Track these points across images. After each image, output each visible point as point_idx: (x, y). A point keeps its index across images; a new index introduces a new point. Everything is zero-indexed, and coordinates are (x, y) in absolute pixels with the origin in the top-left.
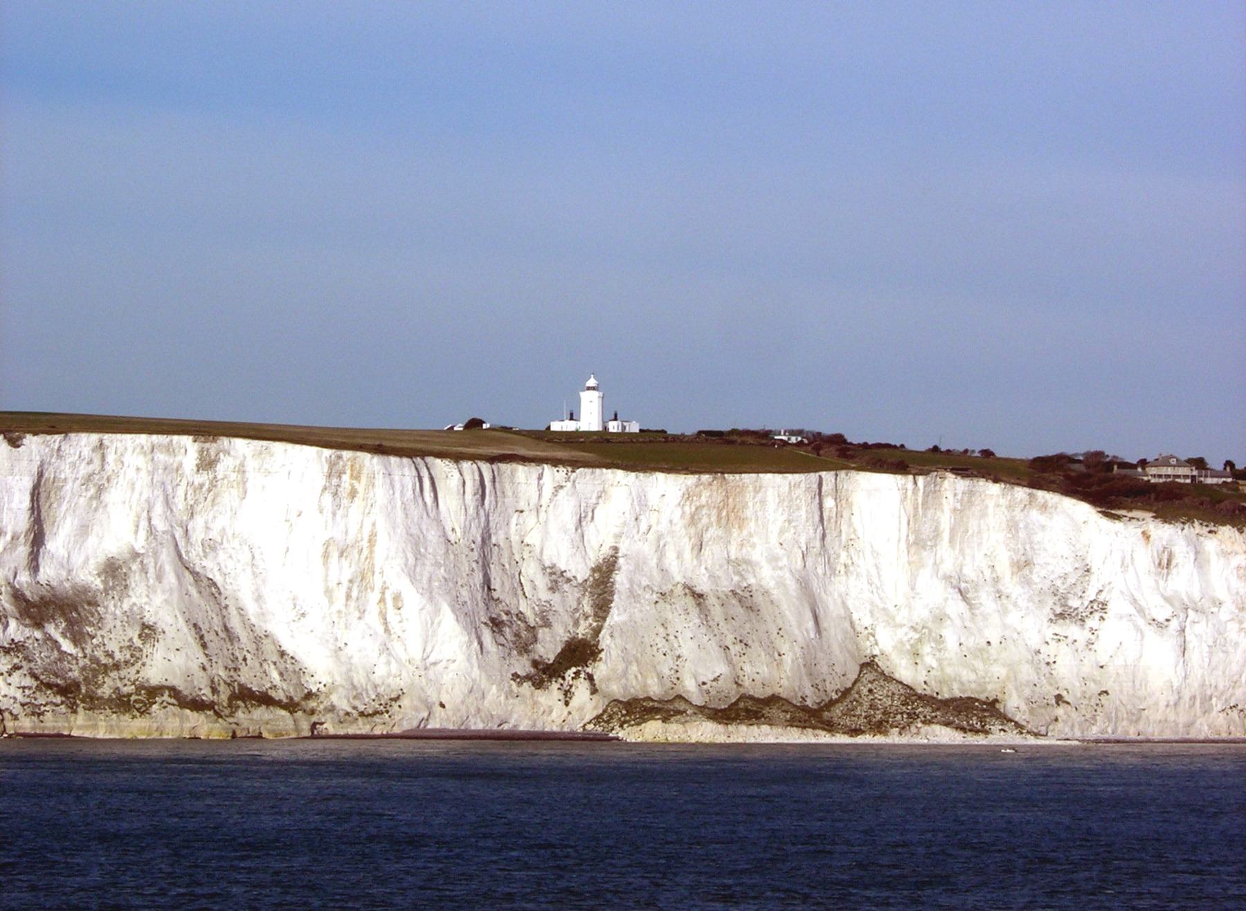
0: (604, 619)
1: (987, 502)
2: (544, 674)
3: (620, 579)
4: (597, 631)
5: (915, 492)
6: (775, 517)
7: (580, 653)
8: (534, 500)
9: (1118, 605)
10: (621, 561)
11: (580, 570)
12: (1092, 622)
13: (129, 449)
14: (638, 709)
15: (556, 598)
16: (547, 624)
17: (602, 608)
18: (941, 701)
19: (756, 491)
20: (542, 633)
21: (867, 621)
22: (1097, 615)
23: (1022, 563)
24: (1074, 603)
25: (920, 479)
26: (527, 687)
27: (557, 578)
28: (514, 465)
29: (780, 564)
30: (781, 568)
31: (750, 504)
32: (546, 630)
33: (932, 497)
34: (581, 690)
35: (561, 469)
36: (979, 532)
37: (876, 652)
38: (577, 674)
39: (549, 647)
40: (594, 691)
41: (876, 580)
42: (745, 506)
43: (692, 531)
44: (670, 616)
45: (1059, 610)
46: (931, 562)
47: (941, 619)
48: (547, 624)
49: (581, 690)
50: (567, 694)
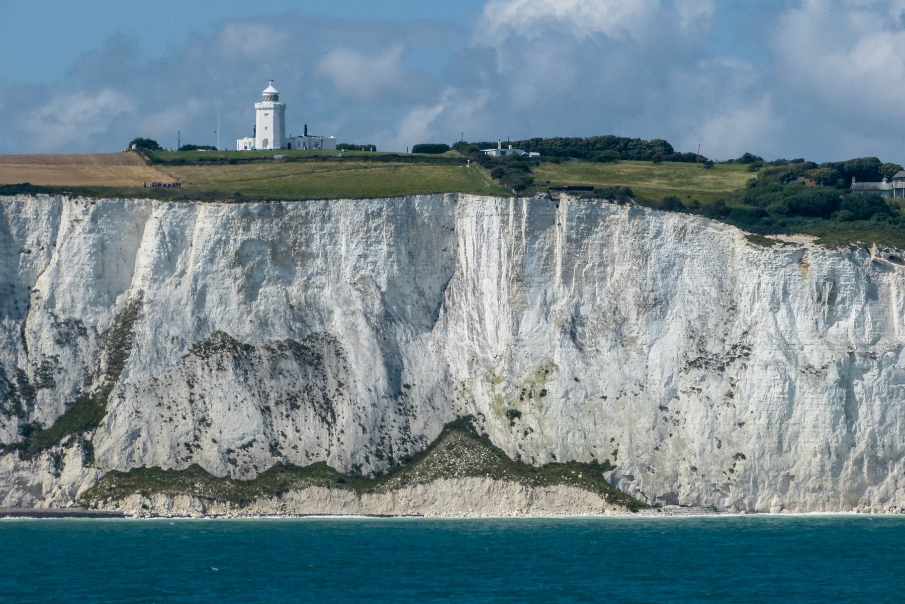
0: (116, 378)
1: (613, 228)
2: (33, 442)
3: (143, 330)
4: (107, 391)
5: (518, 216)
6: (347, 248)
7: (85, 415)
8: (46, 240)
9: (762, 352)
10: (146, 308)
11: (104, 319)
12: (730, 371)
13: (73, 210)
14: (146, 479)
15: (65, 354)
16: (48, 383)
18: (539, 469)
19: (324, 220)
20: (43, 395)
21: (464, 375)
22: (738, 363)
23: (651, 301)
24: (713, 347)
25: (525, 202)
28: (20, 198)
29: (352, 308)
30: (353, 313)
31: (317, 237)
32: (47, 391)
33: (540, 223)
34: (73, 459)
35: (81, 199)
36: (601, 265)
37: (472, 411)
38: (71, 441)
39: (46, 410)
41: (477, 326)
42: (309, 241)
43: (238, 270)
44: (199, 372)
45: (693, 356)
46: (539, 299)
47: (545, 371)
48: (48, 383)
49: (73, 459)
50: (58, 463)
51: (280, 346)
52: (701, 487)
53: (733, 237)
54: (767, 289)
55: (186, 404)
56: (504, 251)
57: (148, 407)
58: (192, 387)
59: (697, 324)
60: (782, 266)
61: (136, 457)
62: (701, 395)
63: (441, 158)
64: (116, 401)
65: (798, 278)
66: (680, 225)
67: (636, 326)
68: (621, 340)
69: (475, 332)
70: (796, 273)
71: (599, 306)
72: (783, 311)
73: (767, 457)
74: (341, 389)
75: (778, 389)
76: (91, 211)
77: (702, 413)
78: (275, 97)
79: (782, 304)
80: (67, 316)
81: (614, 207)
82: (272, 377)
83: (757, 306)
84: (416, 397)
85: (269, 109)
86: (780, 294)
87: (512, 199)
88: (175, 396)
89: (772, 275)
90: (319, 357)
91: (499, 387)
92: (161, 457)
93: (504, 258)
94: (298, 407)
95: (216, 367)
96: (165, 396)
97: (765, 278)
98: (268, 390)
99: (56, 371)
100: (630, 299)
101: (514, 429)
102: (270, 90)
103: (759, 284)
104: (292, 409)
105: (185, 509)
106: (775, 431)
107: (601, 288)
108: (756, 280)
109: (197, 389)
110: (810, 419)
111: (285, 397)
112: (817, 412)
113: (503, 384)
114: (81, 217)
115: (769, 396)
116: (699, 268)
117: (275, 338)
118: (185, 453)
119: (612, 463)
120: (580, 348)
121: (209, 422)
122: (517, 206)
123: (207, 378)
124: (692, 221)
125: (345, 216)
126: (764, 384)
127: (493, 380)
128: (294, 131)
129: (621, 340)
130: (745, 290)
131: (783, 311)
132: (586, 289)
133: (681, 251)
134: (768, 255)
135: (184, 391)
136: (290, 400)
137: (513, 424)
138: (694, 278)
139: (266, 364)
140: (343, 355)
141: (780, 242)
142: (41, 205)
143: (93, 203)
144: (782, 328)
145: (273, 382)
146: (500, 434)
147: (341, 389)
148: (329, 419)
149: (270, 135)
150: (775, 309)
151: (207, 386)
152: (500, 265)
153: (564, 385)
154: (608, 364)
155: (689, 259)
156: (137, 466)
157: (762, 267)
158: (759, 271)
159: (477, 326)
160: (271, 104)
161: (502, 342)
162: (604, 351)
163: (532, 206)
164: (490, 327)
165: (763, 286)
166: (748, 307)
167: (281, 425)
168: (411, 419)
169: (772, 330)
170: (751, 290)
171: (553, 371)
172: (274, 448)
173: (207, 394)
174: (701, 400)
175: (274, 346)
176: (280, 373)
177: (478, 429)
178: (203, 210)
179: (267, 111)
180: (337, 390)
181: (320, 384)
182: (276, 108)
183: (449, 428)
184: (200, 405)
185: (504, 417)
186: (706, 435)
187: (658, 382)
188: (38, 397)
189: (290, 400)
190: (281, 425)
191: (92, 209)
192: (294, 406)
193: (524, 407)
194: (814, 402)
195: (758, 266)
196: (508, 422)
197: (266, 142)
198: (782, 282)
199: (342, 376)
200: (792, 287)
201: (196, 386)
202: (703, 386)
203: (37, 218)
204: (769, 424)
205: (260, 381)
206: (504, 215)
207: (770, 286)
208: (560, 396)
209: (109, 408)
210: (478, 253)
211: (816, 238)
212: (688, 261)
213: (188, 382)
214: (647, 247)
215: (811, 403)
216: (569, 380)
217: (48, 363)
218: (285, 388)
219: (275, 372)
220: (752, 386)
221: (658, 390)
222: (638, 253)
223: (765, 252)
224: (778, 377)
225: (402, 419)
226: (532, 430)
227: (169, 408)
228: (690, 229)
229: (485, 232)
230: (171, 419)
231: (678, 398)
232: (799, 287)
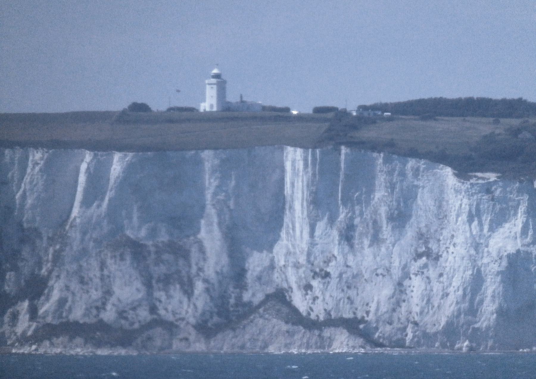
37: (285, 285)
52: (420, 335)
53: (447, 174)
54: (466, 208)
56: (305, 183)
57: (75, 286)
59: (424, 230)
60: (475, 193)
61: (64, 314)
62: (423, 276)
64: (54, 279)
65: (485, 201)
66: (415, 167)
67: (386, 231)
68: (376, 240)
69: (290, 236)
70: (484, 198)
71: (365, 218)
72: (476, 223)
73: (462, 316)
75: (470, 272)
76: (45, 157)
77: (423, 287)
78: (217, 76)
79: (476, 219)
80: (29, 225)
81: (375, 155)
83: (460, 219)
84: (250, 277)
85: (214, 84)
86: (474, 212)
87: (310, 150)
89: (469, 199)
91: (301, 271)
92: (77, 314)
93: (305, 188)
97: (465, 201)
100: (384, 215)
101: (308, 297)
102: (215, 71)
103: (461, 205)
106: (468, 298)
107: (366, 208)
108: (459, 202)
110: (489, 292)
112: (494, 287)
113: (304, 269)
114: (39, 162)
115: (464, 276)
116: (427, 195)
117: (161, 239)
118: (94, 312)
119: (366, 319)
120: (352, 246)
122: (314, 155)
124: (422, 164)
125: (208, 161)
126: (461, 269)
127: (297, 266)
128: (232, 98)
129: (376, 240)
130: (453, 209)
131: (476, 223)
132: (357, 208)
133: (416, 183)
134: (466, 186)
137: (307, 294)
138: (425, 200)
139: (153, 256)
141: (475, 176)
142: (14, 152)
143: (46, 152)
144: (474, 233)
146: (299, 301)
148: (190, 291)
149: (214, 102)
150: (470, 220)
152: (303, 193)
153: (339, 269)
154: (367, 256)
155: (421, 189)
156: (64, 320)
157: (463, 193)
158: (462, 197)
159: (291, 231)
160: (214, 81)
161: (305, 242)
162: (366, 247)
163: (322, 153)
164: (298, 233)
165: (463, 206)
166: (455, 219)
167: (160, 295)
169: (468, 234)
170: (457, 208)
172: (153, 309)
174: (423, 279)
178: (117, 156)
179: (212, 86)
182: (218, 84)
183: (268, 297)
184: (107, 281)
185: (302, 290)
186: (425, 302)
187: (397, 268)
188: (7, 277)
190: (160, 295)
191: (46, 155)
193: (315, 283)
194: (493, 280)
195: (461, 193)
196: (304, 292)
197: (212, 106)
198: (475, 203)
199: (201, 263)
200: (482, 206)
201: (105, 270)
202: (425, 271)
203: (13, 163)
204: (464, 295)
206: (305, 160)
207: (467, 206)
208: (336, 276)
209: (51, 283)
210: (293, 184)
211: (499, 175)
212: (420, 190)
214: (394, 180)
215: (491, 281)
216: (343, 266)
220: (454, 270)
221: (396, 273)
222: (388, 184)
223: (465, 184)
224: (470, 264)
228: (421, 169)
229: (296, 171)
231: (410, 279)
232: (486, 207)
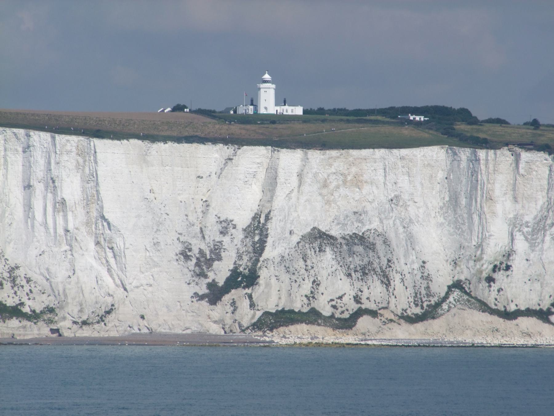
11: (243, 219)
14: (284, 318)
17: (259, 249)
26: (204, 303)
27: (226, 227)
40: (252, 305)
51: (351, 237)
55: (303, 271)
58: (305, 261)
63: (365, 120)
74: (390, 264)
82: (350, 257)
88: (296, 267)
90: (374, 244)
94: (367, 274)
95: (318, 250)
96: (291, 267)
98: (349, 263)
99: (222, 250)
104: (364, 275)
105: (138, 350)
109: (309, 263)
111: (358, 268)
121: (318, 283)
123: (314, 256)
135: (301, 263)
136: (362, 269)
140: (389, 243)
145: (351, 259)
147: (390, 264)
151: (314, 261)
168: (430, 282)
171: (513, 255)
172: (357, 299)
173: (315, 265)
175: (348, 237)
176: (354, 254)
177: (467, 289)
180: (388, 264)
181: (377, 261)
189: (362, 269)
192: (365, 274)
205: (343, 258)
213: (303, 258)
217: (217, 245)
218: (358, 263)
219: (162, 261)
225: (426, 282)
226: (502, 290)
227: (294, 274)
230: (296, 281)
